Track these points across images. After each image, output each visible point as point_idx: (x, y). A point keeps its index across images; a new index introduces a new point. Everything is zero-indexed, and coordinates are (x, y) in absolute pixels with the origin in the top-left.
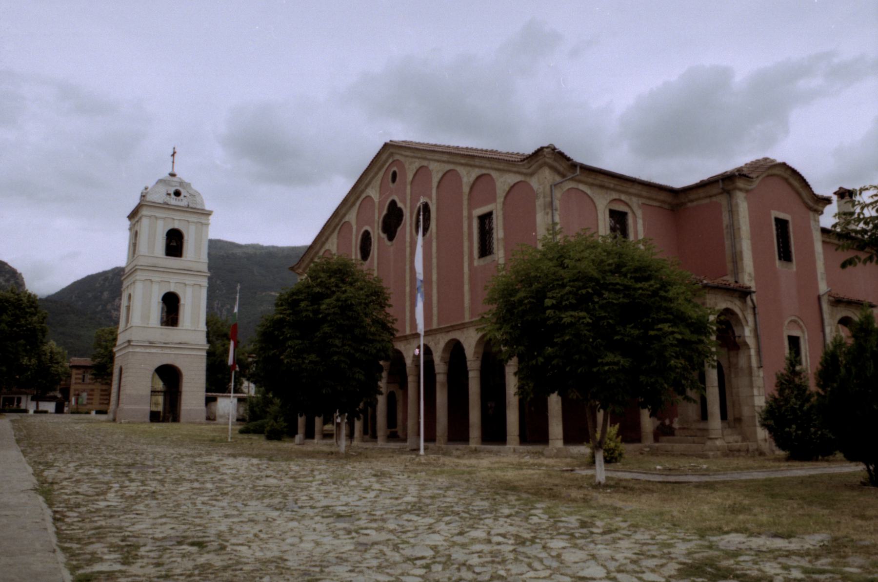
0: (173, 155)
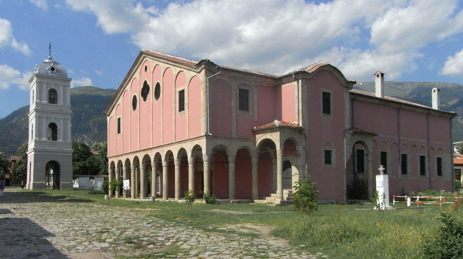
0: (50, 48)
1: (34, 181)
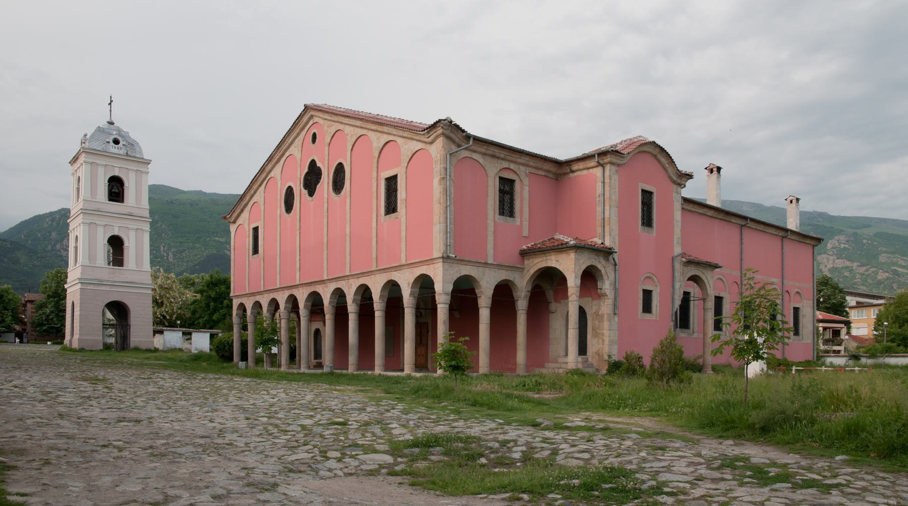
0: (110, 104)
1: (80, 334)
